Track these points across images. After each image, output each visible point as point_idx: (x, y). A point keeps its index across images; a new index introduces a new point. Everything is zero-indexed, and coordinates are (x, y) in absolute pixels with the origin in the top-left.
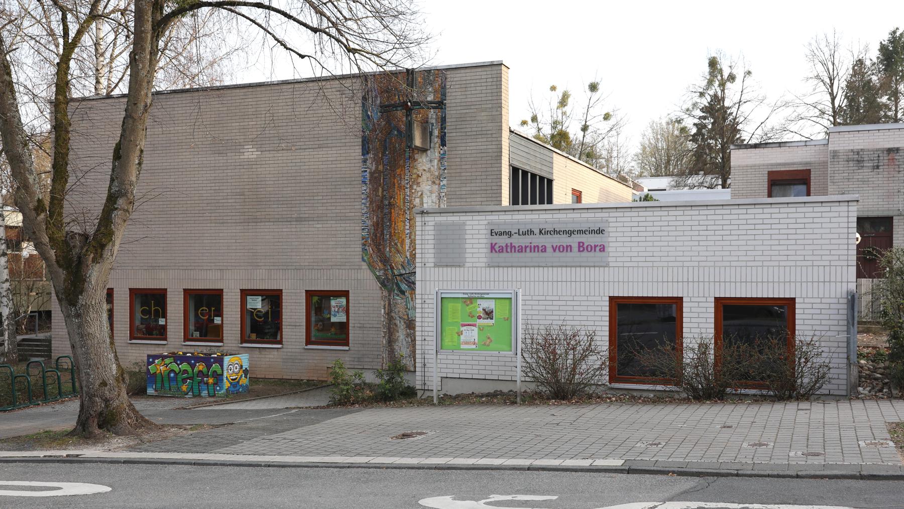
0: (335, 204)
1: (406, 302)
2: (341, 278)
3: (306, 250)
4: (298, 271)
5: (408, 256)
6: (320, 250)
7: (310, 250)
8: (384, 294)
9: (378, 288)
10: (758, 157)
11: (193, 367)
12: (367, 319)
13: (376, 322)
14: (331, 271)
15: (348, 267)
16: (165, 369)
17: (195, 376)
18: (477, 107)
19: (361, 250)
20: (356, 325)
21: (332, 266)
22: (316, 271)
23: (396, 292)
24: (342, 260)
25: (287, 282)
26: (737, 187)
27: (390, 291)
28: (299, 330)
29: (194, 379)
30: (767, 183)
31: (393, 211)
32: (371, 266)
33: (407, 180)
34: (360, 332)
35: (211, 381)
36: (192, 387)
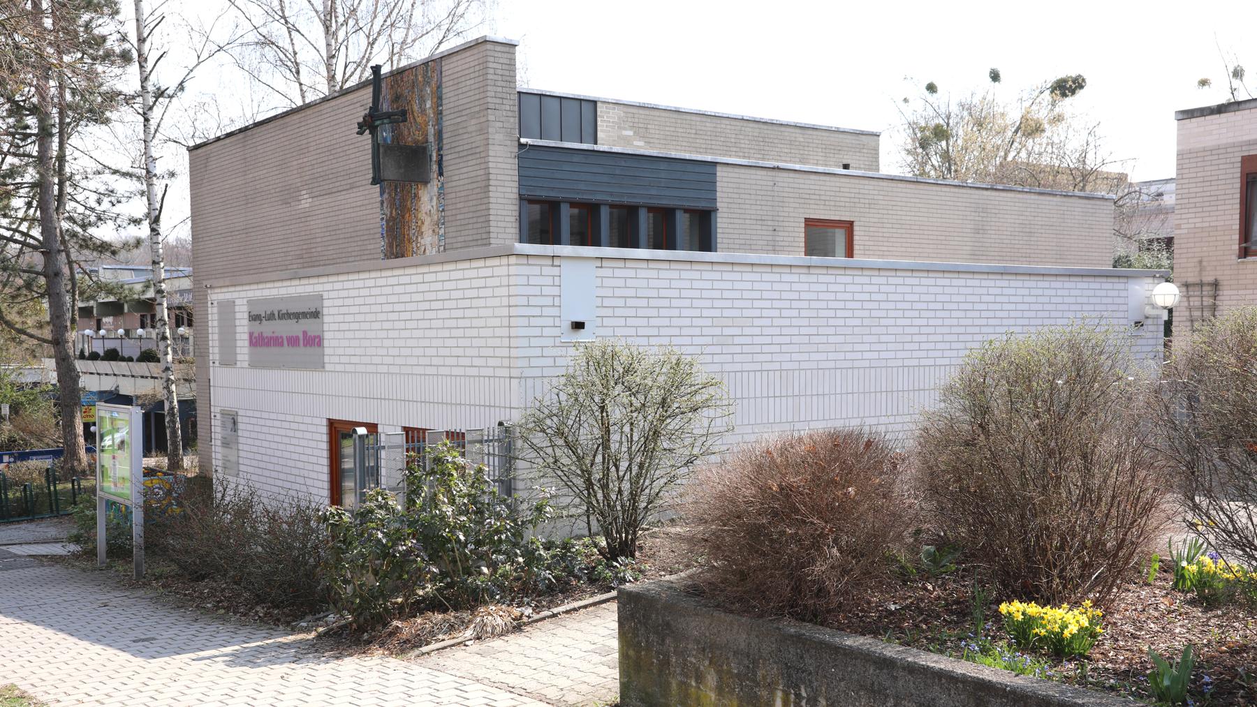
10: (1225, 130)
18: (468, 111)
26: (1186, 191)
30: (1239, 180)
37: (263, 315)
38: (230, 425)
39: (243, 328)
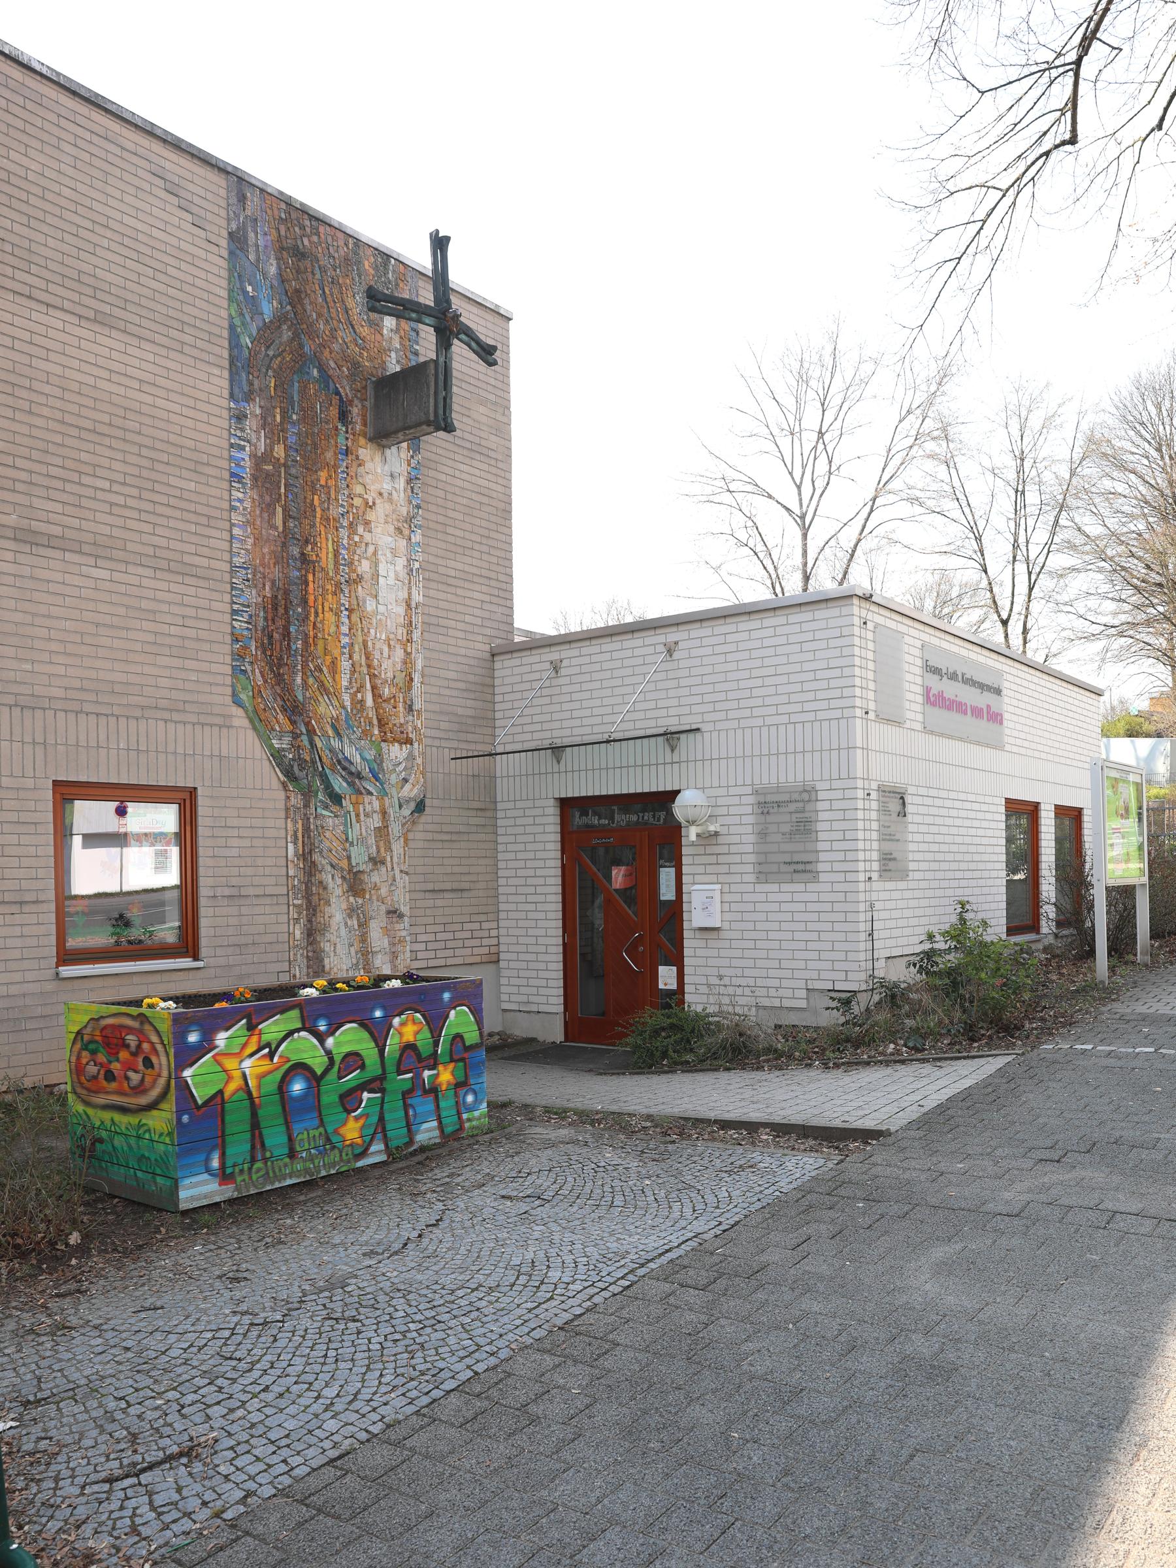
0: (152, 518)
1: (345, 825)
2: (171, 748)
3: (54, 646)
4: (28, 713)
5: (348, 704)
6: (101, 652)
7: (70, 648)
8: (293, 801)
9: (276, 784)
11: (378, 1034)
12: (249, 871)
13: (272, 881)
14: (142, 723)
15: (194, 719)
16: (266, 1066)
17: (391, 1068)
19: (228, 670)
20: (219, 891)
21: (143, 708)
22: (92, 718)
23: (320, 796)
24: (175, 695)
25: (82, 738)
27: (308, 794)
28: (33, 919)
29: (388, 1086)
31: (310, 577)
32: (259, 721)
33: (342, 506)
34: (233, 910)
35: (445, 1076)
36: (381, 1119)
37: (944, 671)
38: (895, 806)
39: (913, 683)
